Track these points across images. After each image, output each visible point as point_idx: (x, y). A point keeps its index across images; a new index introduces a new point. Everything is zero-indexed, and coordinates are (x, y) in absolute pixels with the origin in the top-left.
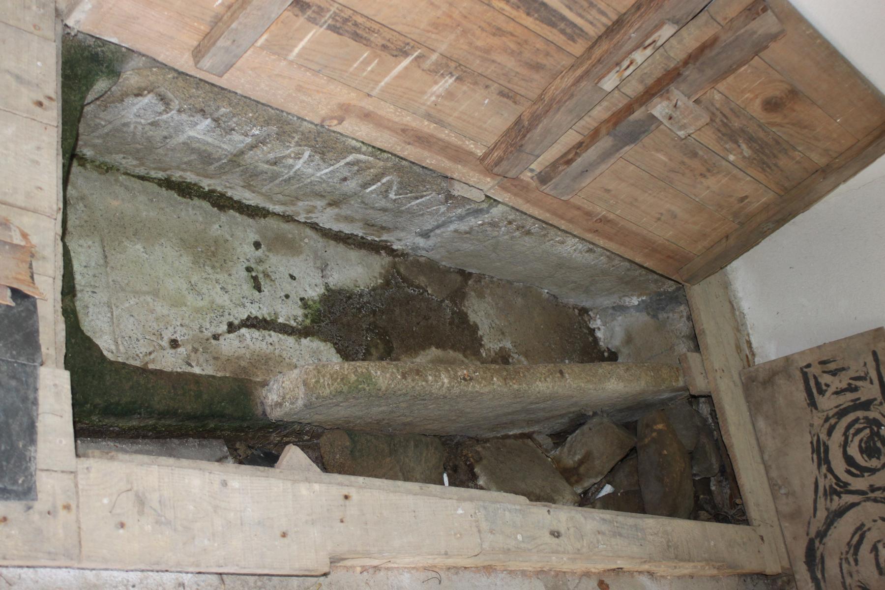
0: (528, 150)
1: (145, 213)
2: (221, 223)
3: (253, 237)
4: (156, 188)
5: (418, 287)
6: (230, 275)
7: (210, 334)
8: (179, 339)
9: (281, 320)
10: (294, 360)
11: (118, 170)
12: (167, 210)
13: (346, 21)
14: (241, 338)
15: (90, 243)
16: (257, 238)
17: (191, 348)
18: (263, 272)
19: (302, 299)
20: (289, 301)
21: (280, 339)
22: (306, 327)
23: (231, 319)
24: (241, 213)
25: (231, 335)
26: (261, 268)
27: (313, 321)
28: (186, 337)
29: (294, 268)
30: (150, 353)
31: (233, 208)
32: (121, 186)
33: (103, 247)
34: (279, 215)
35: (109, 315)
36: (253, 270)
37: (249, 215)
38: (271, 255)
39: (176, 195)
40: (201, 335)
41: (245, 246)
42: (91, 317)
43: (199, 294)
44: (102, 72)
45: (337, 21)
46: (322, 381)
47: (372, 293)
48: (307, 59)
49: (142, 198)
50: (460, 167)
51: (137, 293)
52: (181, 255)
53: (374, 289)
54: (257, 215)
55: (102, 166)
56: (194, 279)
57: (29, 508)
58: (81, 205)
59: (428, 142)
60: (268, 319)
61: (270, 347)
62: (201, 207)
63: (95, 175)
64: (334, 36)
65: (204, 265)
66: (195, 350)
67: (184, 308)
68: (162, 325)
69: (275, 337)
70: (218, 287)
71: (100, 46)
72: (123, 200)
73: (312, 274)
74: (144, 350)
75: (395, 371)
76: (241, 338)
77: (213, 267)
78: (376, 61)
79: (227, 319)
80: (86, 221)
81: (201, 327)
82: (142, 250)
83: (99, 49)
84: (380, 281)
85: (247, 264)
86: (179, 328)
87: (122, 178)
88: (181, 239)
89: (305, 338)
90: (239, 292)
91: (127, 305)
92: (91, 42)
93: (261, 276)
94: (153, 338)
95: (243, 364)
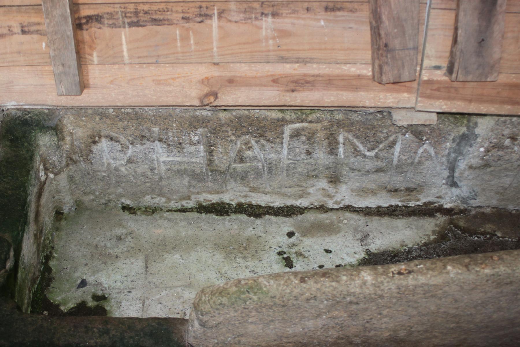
0: (398, 47)
4: (196, 215)
5: (484, 233)
11: (161, 210)
12: (205, 227)
13: (136, 13)
16: (291, 229)
26: (293, 250)
31: (268, 213)
32: (165, 220)
35: (141, 305)
36: (285, 253)
39: (214, 216)
41: (278, 237)
44: (33, 129)
45: (130, 17)
47: (423, 248)
48: (139, 57)
50: (362, 93)
52: (214, 255)
53: (425, 245)
54: (294, 214)
55: (148, 210)
58: (129, 238)
59: (308, 82)
64: (141, 30)
65: (235, 258)
71: (27, 115)
72: (165, 228)
73: (351, 246)
77: (244, 258)
78: (191, 34)
80: (132, 248)
82: (179, 257)
83: (27, 116)
84: (432, 237)
85: (279, 250)
88: (215, 244)
91: (158, 296)
92: (20, 114)
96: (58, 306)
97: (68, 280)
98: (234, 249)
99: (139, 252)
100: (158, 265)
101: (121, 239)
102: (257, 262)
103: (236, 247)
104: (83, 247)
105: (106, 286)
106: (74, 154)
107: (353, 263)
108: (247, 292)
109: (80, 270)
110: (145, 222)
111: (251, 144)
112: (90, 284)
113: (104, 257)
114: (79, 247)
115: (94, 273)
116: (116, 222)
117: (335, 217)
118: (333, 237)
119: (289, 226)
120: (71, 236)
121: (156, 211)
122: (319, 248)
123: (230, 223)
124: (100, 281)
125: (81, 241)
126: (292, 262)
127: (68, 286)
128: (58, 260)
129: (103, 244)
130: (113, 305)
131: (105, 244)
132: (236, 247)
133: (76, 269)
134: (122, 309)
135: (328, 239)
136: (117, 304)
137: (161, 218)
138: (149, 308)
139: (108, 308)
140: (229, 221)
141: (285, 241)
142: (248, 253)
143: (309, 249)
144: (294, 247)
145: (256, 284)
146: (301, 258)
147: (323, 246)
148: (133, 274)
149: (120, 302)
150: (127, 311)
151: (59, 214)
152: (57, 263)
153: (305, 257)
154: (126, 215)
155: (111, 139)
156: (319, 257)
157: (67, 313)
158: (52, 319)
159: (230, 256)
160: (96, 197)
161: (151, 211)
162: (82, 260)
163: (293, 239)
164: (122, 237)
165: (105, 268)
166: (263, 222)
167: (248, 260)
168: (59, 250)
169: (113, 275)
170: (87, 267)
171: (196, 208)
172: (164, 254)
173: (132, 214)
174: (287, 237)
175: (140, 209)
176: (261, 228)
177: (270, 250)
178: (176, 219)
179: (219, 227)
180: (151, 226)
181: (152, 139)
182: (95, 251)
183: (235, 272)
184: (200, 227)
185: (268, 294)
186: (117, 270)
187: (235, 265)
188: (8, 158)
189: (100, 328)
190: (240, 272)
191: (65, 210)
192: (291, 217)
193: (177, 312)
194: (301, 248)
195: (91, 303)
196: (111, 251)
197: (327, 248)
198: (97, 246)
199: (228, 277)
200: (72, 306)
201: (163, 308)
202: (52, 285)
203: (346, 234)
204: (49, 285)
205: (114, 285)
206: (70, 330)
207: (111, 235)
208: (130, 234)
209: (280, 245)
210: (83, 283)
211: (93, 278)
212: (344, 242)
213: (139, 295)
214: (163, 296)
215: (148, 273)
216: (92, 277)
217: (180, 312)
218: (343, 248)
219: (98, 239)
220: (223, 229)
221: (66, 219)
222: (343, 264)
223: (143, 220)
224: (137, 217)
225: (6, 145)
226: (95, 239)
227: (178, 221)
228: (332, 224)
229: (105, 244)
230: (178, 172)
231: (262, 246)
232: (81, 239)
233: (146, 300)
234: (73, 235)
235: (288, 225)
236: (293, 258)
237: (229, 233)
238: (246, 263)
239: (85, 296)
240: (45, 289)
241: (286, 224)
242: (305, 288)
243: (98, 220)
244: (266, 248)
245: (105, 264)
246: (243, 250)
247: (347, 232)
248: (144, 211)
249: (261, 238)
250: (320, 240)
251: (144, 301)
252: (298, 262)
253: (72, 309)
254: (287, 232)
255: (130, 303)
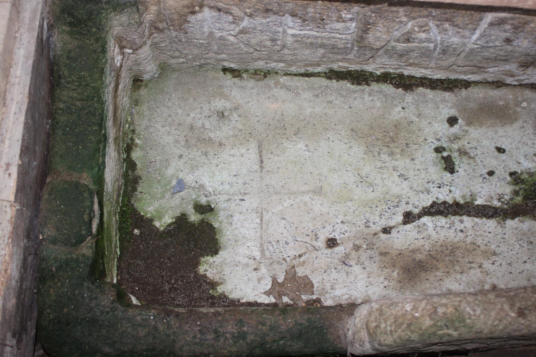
1: (309, 110)
2: (404, 105)
3: (448, 112)
4: (324, 82)
6: (413, 159)
7: (379, 229)
8: (337, 237)
9: (479, 202)
10: (493, 247)
12: (337, 102)
14: (421, 229)
15: (244, 151)
16: (453, 112)
17: (352, 245)
18: (459, 150)
19: (511, 174)
20: (494, 178)
21: (476, 224)
22: (515, 206)
23: (410, 208)
24: (433, 88)
25: (408, 227)
26: (455, 146)
27: (526, 198)
28: (347, 235)
29: (504, 139)
30: (300, 256)
32: (282, 88)
33: (260, 152)
34: (481, 82)
35: (258, 221)
36: (444, 149)
37: (445, 89)
38: (471, 129)
39: (349, 85)
40: (367, 231)
41: (436, 125)
42: (235, 226)
43: (371, 185)
46: (383, 325)
49: (307, 95)
51: (291, 194)
52: (351, 147)
55: (258, 72)
56: (366, 169)
57: (506, 285)
60: (462, 202)
61: (460, 234)
62: (381, 92)
63: (251, 83)
65: (379, 154)
66: (357, 248)
67: (349, 204)
68: (319, 225)
69: (468, 221)
70: (396, 174)
72: (283, 101)
73: (530, 142)
74: (292, 253)
75: (506, 307)
76: (421, 229)
77: (391, 154)
79: (404, 208)
80: (240, 130)
81: (368, 221)
82: (304, 148)
85: (437, 144)
86: (339, 227)
87: (283, 80)
88: (352, 130)
89: (513, 218)
90: (423, 176)
91: (281, 208)
93: (455, 155)
94: (308, 239)
95: (419, 257)
96: (151, 220)
97: (159, 181)
98: (378, 139)
99: (250, 137)
100: (276, 159)
101: (223, 115)
102: (408, 161)
103: (380, 136)
104: (173, 128)
105: (211, 190)
106: (161, 22)
107: (532, 171)
108: (445, 328)
109: (173, 164)
110: (255, 91)
111: (429, 26)
112: (189, 187)
113: (201, 142)
114: (168, 128)
115: (194, 168)
116: (216, 90)
117: (511, 96)
118: (509, 129)
119: (450, 108)
120: (155, 111)
121: (270, 74)
122: (489, 144)
123: (371, 98)
124: (201, 182)
125: (170, 119)
126: (454, 164)
127: (160, 191)
128: (142, 149)
129: (200, 124)
130: (223, 220)
131: (203, 124)
132: (380, 136)
133: (167, 162)
134: (235, 226)
135: (501, 131)
136: (227, 218)
137: (277, 84)
138: (270, 225)
139: (216, 225)
140: (370, 95)
141: (445, 131)
142: (396, 147)
143: (476, 145)
144: (457, 140)
145: (457, 314)
146: (465, 159)
147: (494, 141)
148: (245, 171)
149: (232, 216)
150: (241, 229)
151: (137, 82)
152: (142, 154)
153: (470, 157)
154: (228, 80)
155: (219, 10)
156: (488, 159)
157: (163, 232)
158: (169, 319)
159: (372, 149)
160: (189, 60)
161: (263, 74)
162: (174, 148)
163: (455, 129)
164: (226, 114)
165: (206, 161)
166: (416, 97)
167: (396, 157)
168: (142, 133)
169: (217, 173)
170: (182, 161)
171: (325, 73)
172: (284, 141)
173: (236, 77)
174: (447, 125)
175: (247, 71)
176: (412, 108)
177: (425, 144)
178: (297, 88)
179: (356, 102)
180: (263, 97)
181: (281, 13)
182: (190, 134)
183: (380, 175)
184: (330, 102)
185: (472, 328)
186: (223, 165)
187: (379, 164)
188: (70, 51)
189: (234, 333)
190: (385, 176)
191: (146, 77)
192: (453, 91)
193: (307, 233)
194: (466, 143)
195: (194, 217)
196: (212, 135)
197: (499, 146)
198: (192, 128)
199: (371, 181)
200: (170, 221)
201: (288, 227)
202: (139, 189)
203: (525, 125)
204: (135, 189)
205: (221, 188)
206: (195, 337)
207: (210, 110)
208: (236, 109)
209: (438, 137)
210: (181, 185)
211: (192, 177)
212: (522, 138)
213: (255, 205)
214: (286, 208)
215: (264, 170)
216: (190, 176)
217: (310, 234)
218: (520, 146)
219: (192, 115)
220: (361, 106)
221: (146, 86)
222: (519, 172)
223: (253, 88)
224: (244, 83)
225: (64, 31)
226: (189, 115)
227: (300, 91)
228: (506, 107)
229: (203, 124)
230: (311, 44)
231: (414, 136)
232: (170, 116)
233: (264, 213)
234: (158, 110)
235: (449, 105)
236: (455, 158)
237: (371, 114)
238: (393, 162)
239: (184, 205)
240: (132, 196)
241: (445, 104)
242: (523, 324)
243: (190, 87)
244: (420, 140)
245: (206, 156)
246: (389, 142)
247: (526, 122)
248: (253, 74)
249: (413, 125)
250: (490, 133)
251: (262, 213)
252: (462, 165)
253: (169, 225)
254: (448, 116)
255: (244, 218)
